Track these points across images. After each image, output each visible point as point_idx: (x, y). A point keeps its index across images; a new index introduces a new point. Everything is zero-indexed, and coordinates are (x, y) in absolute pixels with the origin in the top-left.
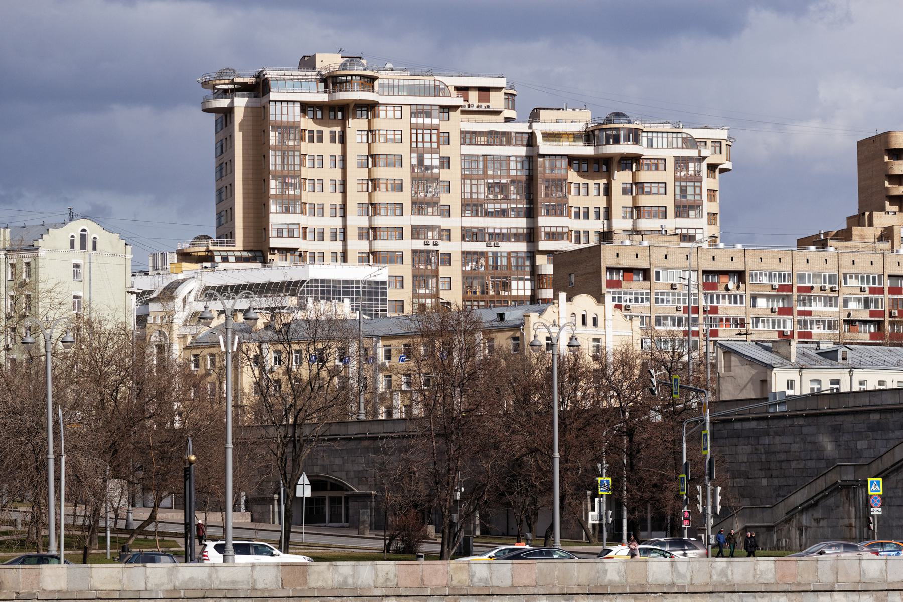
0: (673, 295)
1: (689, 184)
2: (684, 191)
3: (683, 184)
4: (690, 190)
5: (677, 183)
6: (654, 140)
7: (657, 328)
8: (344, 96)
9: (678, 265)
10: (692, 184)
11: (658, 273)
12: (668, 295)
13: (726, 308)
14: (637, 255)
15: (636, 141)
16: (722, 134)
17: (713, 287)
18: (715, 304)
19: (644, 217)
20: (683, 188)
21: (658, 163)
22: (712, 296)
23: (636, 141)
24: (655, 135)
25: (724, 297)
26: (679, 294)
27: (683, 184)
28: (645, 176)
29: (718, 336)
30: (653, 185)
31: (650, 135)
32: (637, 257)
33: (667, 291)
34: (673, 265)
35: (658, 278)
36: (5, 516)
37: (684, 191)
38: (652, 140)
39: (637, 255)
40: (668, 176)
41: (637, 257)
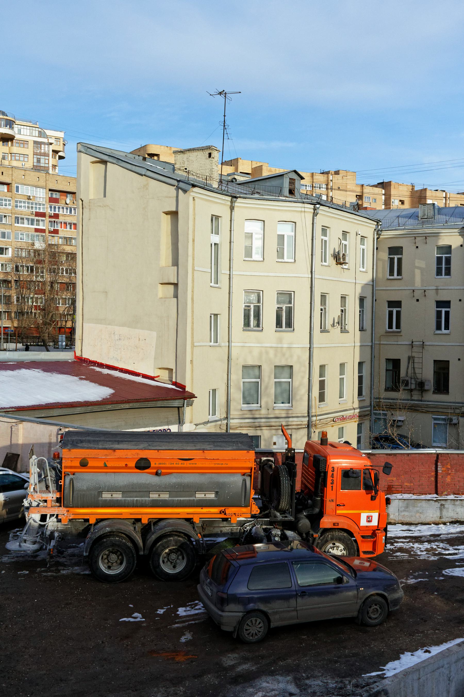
0: (28, 203)
1: (42, 157)
2: (39, 161)
3: (39, 157)
4: (42, 161)
5: (35, 156)
6: (22, 130)
7: (16, 225)
8: (111, 534)
9: (32, 183)
10: (43, 157)
11: (17, 188)
12: (24, 202)
13: (64, 216)
14: (2, 173)
15: (11, 127)
16: (61, 135)
17: (56, 201)
18: (57, 212)
19: (46, 443)
20: (38, 159)
21: (24, 143)
22: (55, 208)
23: (11, 127)
24: (22, 127)
25: (63, 208)
26: (32, 204)
27: (39, 157)
28: (16, 149)
29: (58, 218)
30: (21, 155)
31: (19, 126)
32: (2, 174)
33: (24, 200)
34: (28, 183)
35: (17, 191)
36: (463, 405)
37: (39, 161)
38: (20, 130)
39: (2, 173)
40: (30, 150)
41: (2, 174)
